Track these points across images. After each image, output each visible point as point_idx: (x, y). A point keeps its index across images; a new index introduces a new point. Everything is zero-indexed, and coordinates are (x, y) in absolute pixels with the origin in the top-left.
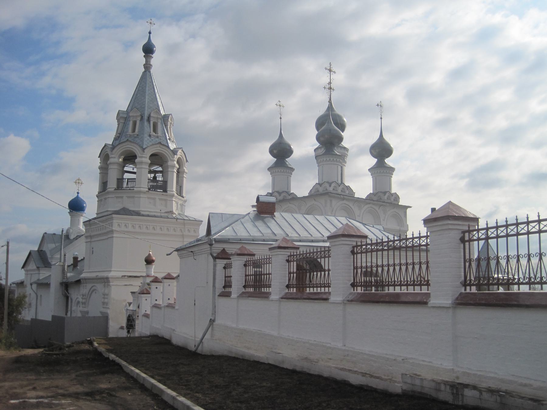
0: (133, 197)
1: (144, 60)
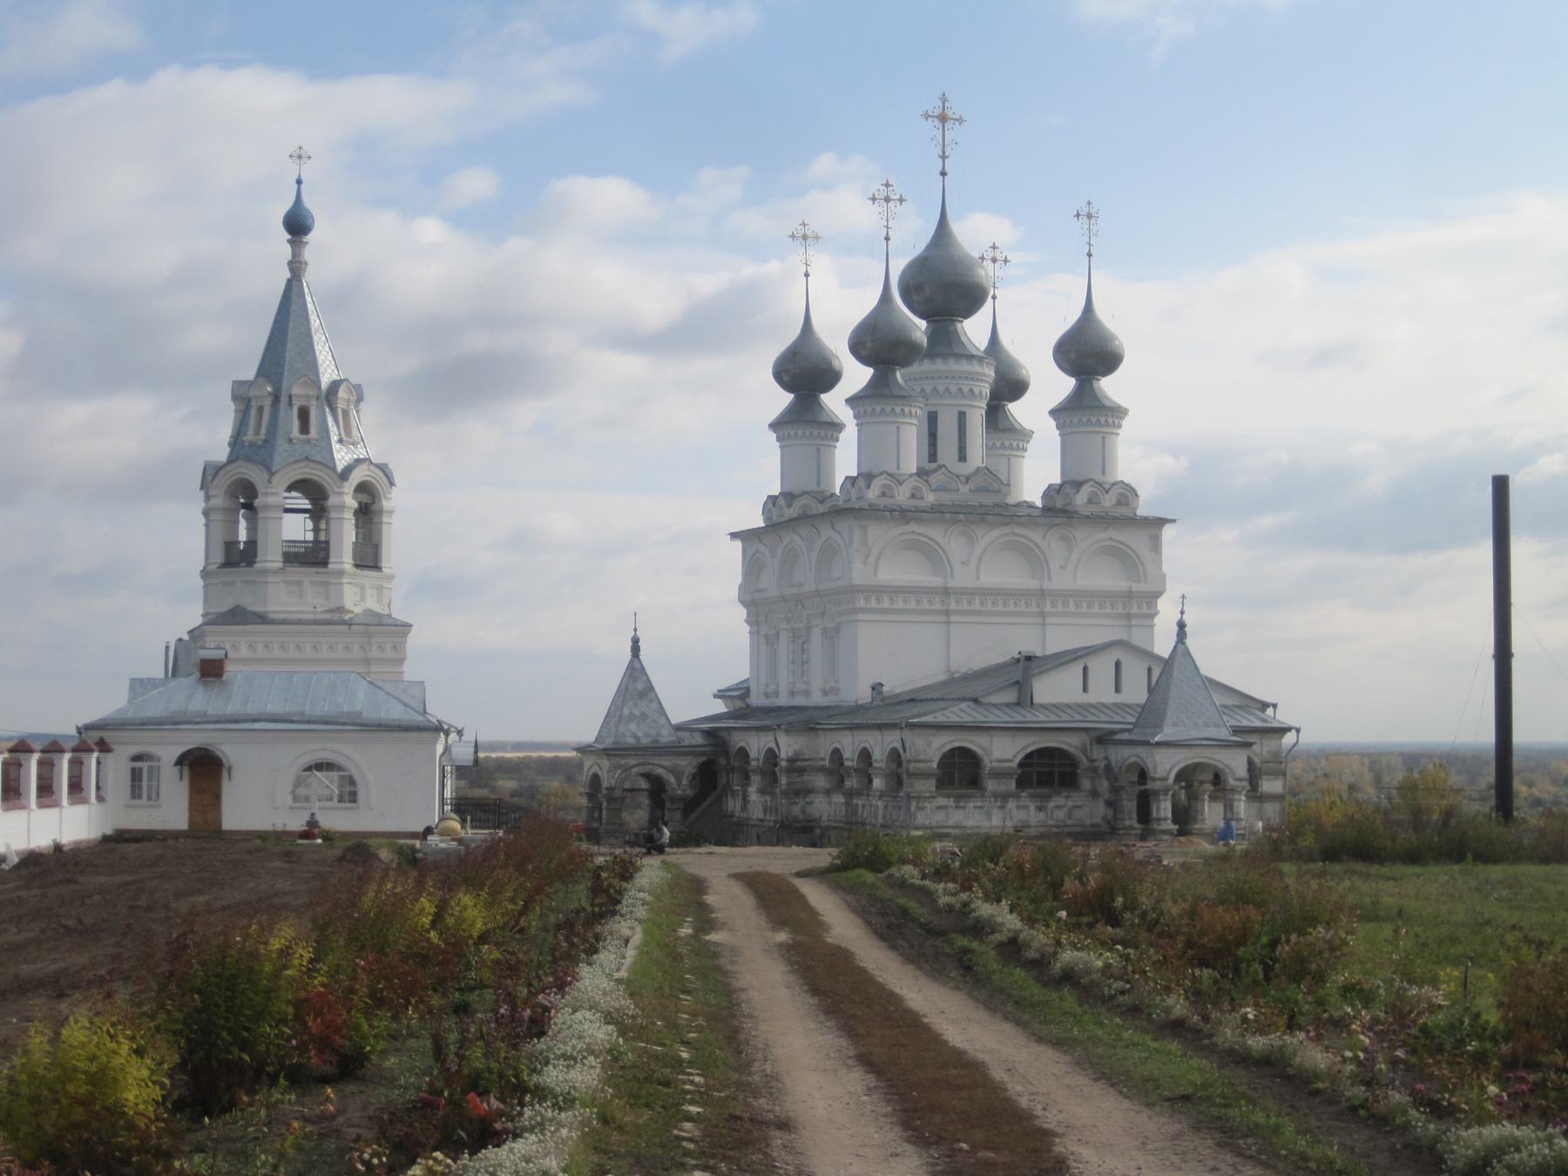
0: (254, 582)
1: (286, 251)
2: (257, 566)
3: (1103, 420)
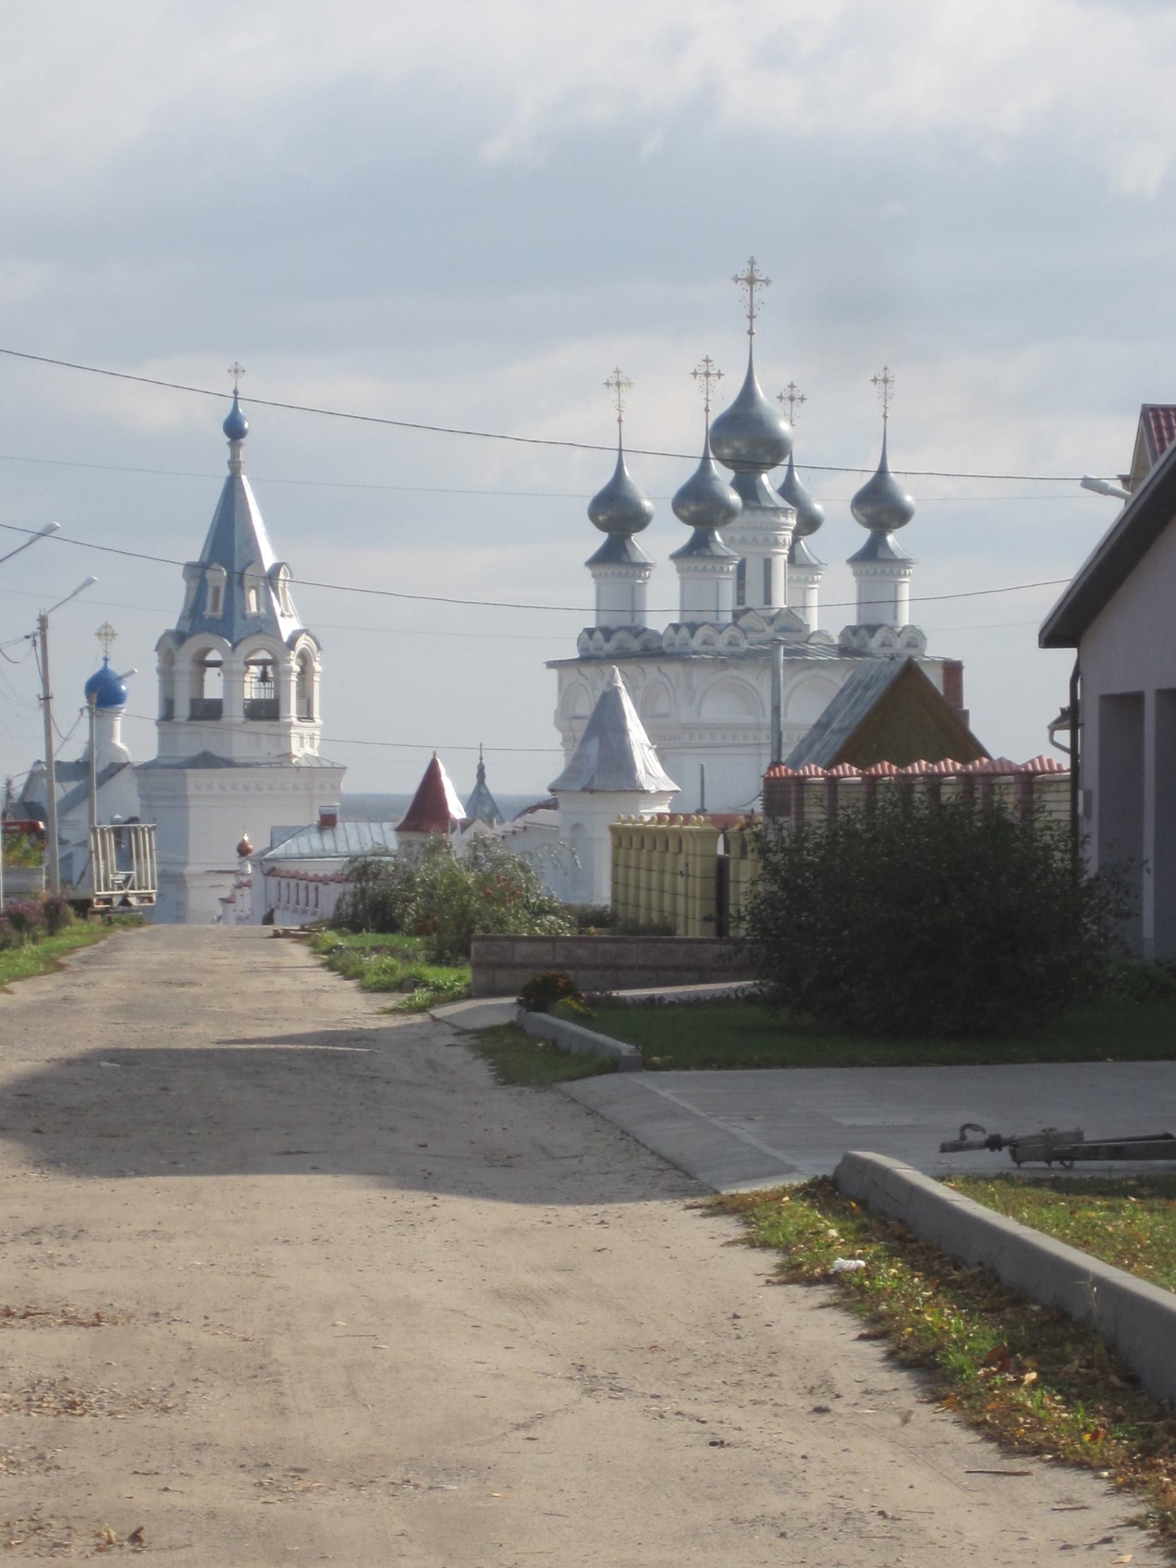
2: (223, 720)
3: (895, 571)
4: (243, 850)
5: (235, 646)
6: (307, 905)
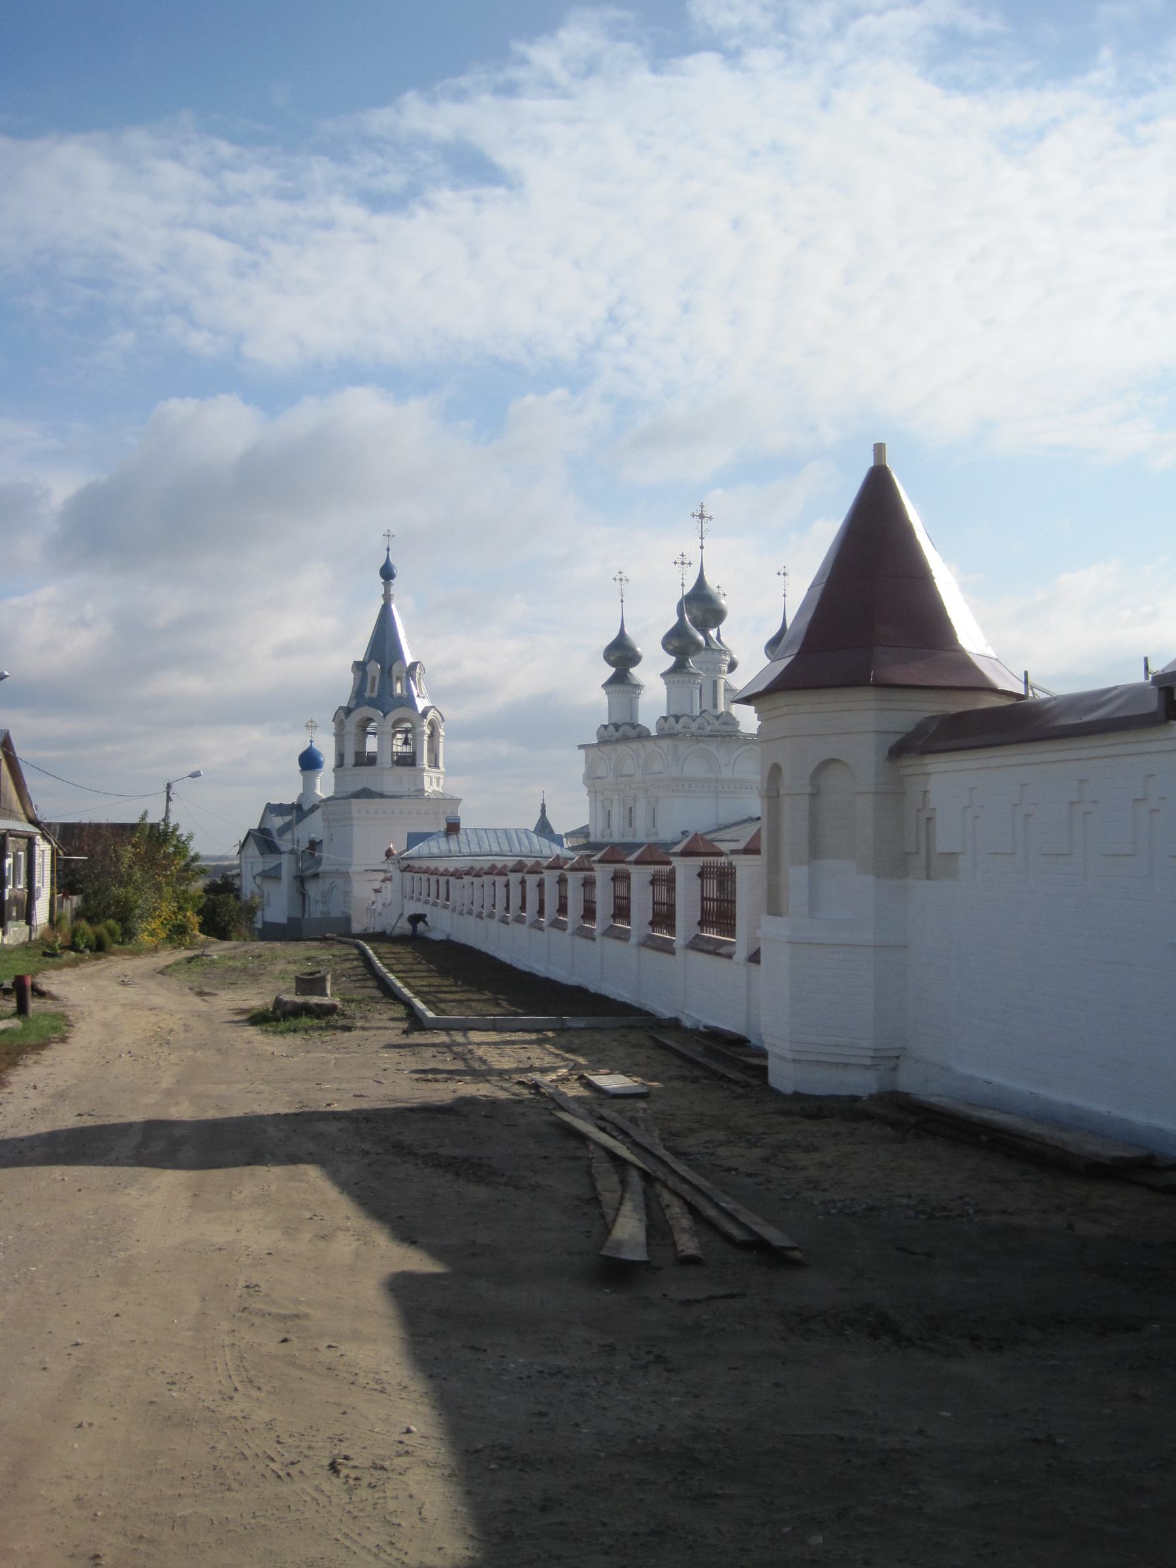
4: (389, 853)
5: (385, 715)
6: (438, 897)
